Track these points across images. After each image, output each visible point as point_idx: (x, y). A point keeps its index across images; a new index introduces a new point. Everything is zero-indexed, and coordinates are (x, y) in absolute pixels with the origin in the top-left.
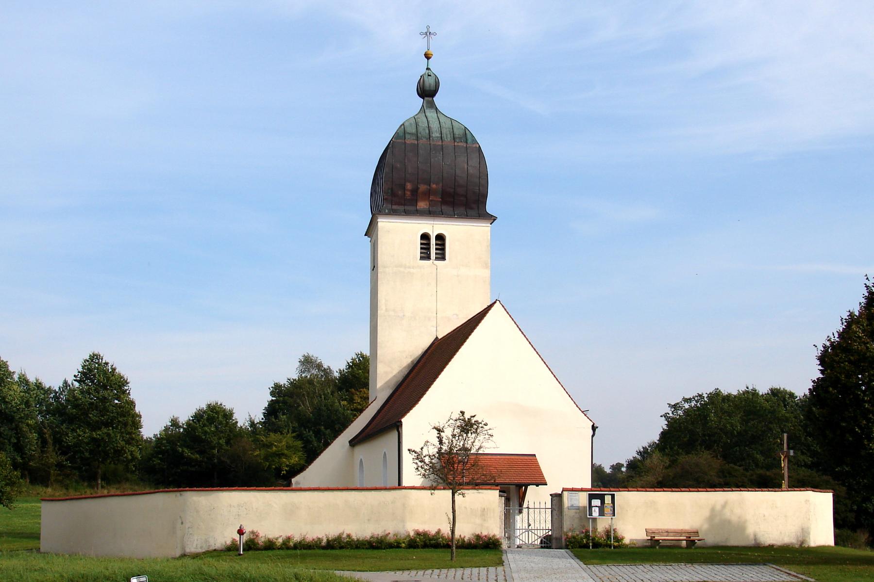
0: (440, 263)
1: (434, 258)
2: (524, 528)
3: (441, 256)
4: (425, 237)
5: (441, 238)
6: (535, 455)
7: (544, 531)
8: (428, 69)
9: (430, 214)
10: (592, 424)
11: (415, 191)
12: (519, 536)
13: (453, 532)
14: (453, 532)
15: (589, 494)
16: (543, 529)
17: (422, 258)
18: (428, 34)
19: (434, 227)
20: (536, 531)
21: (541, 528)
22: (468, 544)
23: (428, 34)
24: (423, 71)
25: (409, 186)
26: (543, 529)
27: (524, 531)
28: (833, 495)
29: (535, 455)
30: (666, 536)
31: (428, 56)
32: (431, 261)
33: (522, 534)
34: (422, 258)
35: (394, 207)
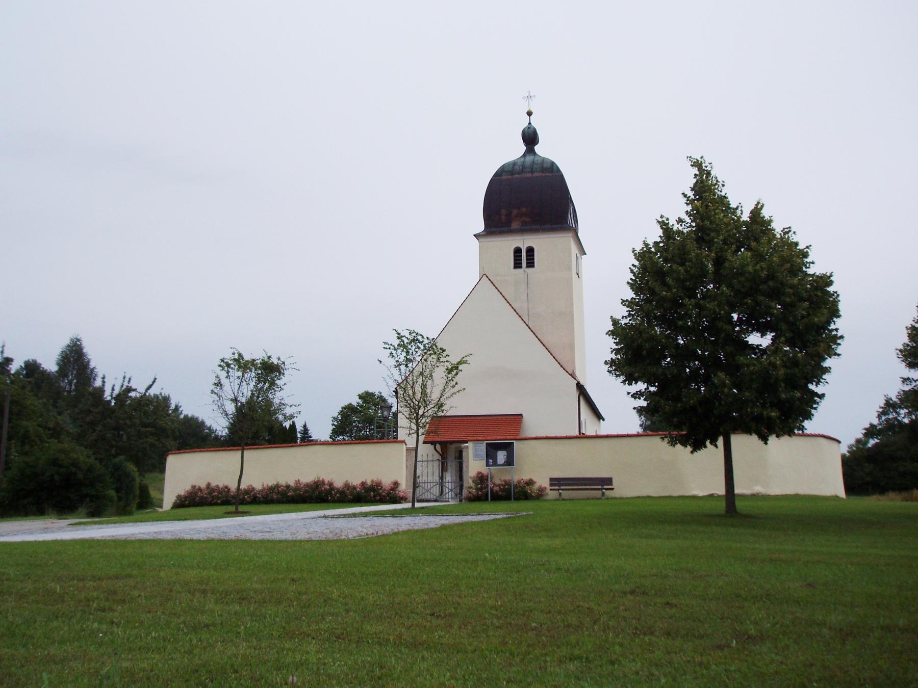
0: (530, 270)
1: (525, 266)
2: (434, 481)
3: (531, 264)
4: (518, 251)
5: (530, 251)
6: (522, 414)
7: (429, 484)
8: (530, 123)
9: (523, 230)
10: (576, 382)
11: (509, 215)
12: (430, 489)
13: (242, 454)
14: (242, 454)
15: (486, 443)
16: (425, 483)
17: (515, 267)
18: (529, 97)
19: (523, 242)
20: (447, 484)
21: (429, 481)
22: (370, 486)
23: (529, 97)
24: (526, 124)
25: (504, 212)
26: (427, 483)
27: (435, 484)
28: (734, 433)
29: (522, 414)
30: (436, 501)
31: (530, 114)
32: (522, 270)
33: (433, 487)
34: (515, 267)
35: (492, 230)
